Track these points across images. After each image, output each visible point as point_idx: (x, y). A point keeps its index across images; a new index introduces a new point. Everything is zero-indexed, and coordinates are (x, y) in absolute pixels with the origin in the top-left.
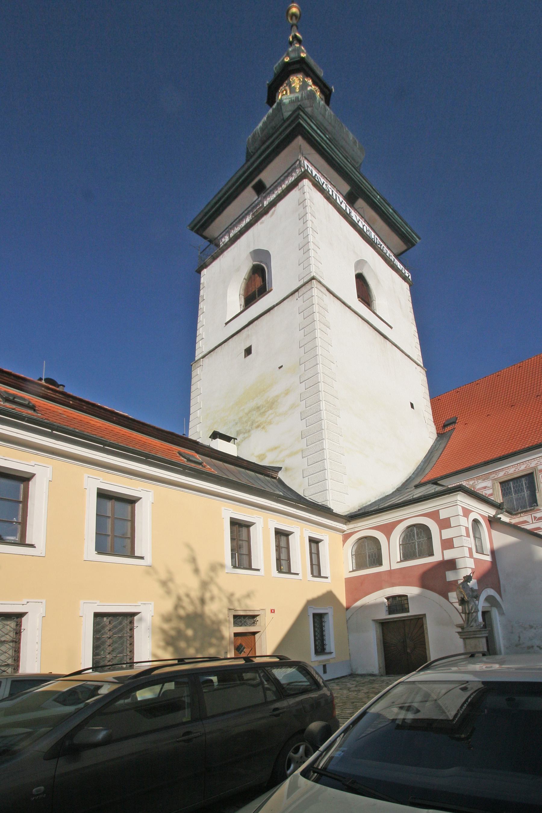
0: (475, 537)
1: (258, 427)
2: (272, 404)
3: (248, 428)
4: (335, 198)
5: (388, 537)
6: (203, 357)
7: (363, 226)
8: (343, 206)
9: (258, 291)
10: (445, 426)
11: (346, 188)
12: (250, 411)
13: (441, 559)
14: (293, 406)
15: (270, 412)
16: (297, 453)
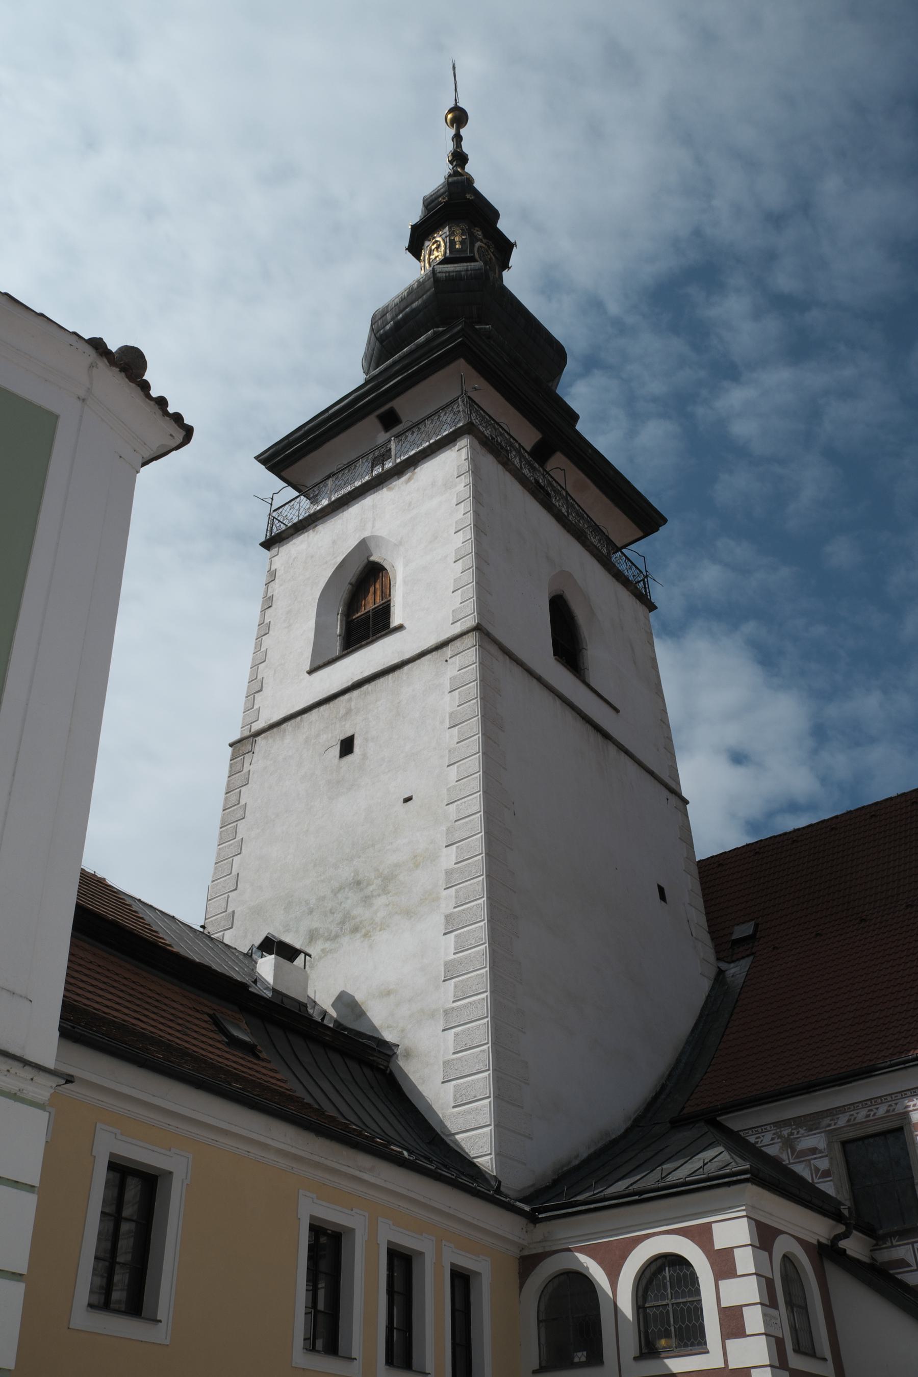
0: (790, 1304)
1: (355, 930)
12: (341, 888)
16: (432, 1015)
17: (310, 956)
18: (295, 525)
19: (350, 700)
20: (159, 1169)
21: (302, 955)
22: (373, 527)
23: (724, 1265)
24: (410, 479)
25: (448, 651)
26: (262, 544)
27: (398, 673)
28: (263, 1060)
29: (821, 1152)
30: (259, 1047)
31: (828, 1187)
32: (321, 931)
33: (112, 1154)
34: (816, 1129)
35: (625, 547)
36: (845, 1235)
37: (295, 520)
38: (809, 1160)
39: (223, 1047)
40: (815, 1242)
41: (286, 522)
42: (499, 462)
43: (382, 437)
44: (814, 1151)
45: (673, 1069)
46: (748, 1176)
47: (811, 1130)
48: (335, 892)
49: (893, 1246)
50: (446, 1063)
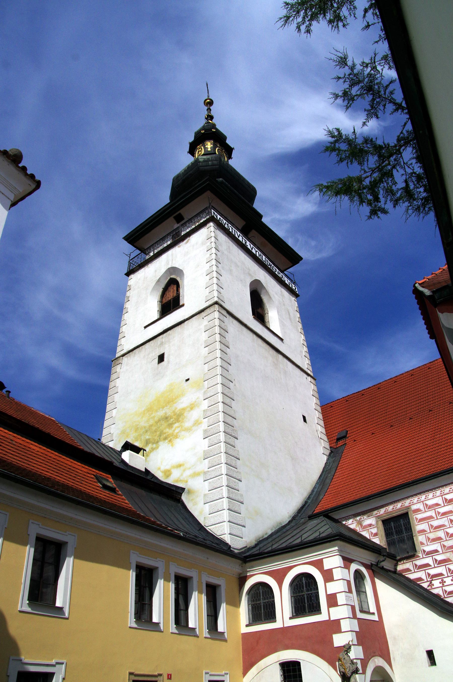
1: (165, 439)
2: (179, 417)
3: (156, 438)
4: (234, 233)
5: (280, 584)
6: (123, 355)
7: (256, 252)
8: (240, 239)
9: (173, 301)
10: (338, 439)
11: (242, 223)
12: (159, 420)
13: (327, 618)
14: (197, 423)
15: (177, 425)
17: (146, 451)
18: (139, 265)
19: (162, 338)
20: (63, 541)
21: (142, 451)
22: (172, 263)
23: (328, 576)
24: (187, 242)
25: (203, 314)
26: (125, 274)
27: (183, 325)
28: (119, 495)
29: (373, 525)
30: (117, 489)
31: (376, 540)
32: (151, 440)
33: (37, 534)
34: (371, 516)
35: (285, 270)
37: (140, 263)
38: (368, 530)
39: (100, 489)
40: (370, 564)
41: (136, 264)
43: (176, 226)
44: (370, 525)
45: (311, 494)
47: (369, 516)
48: (157, 423)
49: (404, 563)
50: (205, 495)
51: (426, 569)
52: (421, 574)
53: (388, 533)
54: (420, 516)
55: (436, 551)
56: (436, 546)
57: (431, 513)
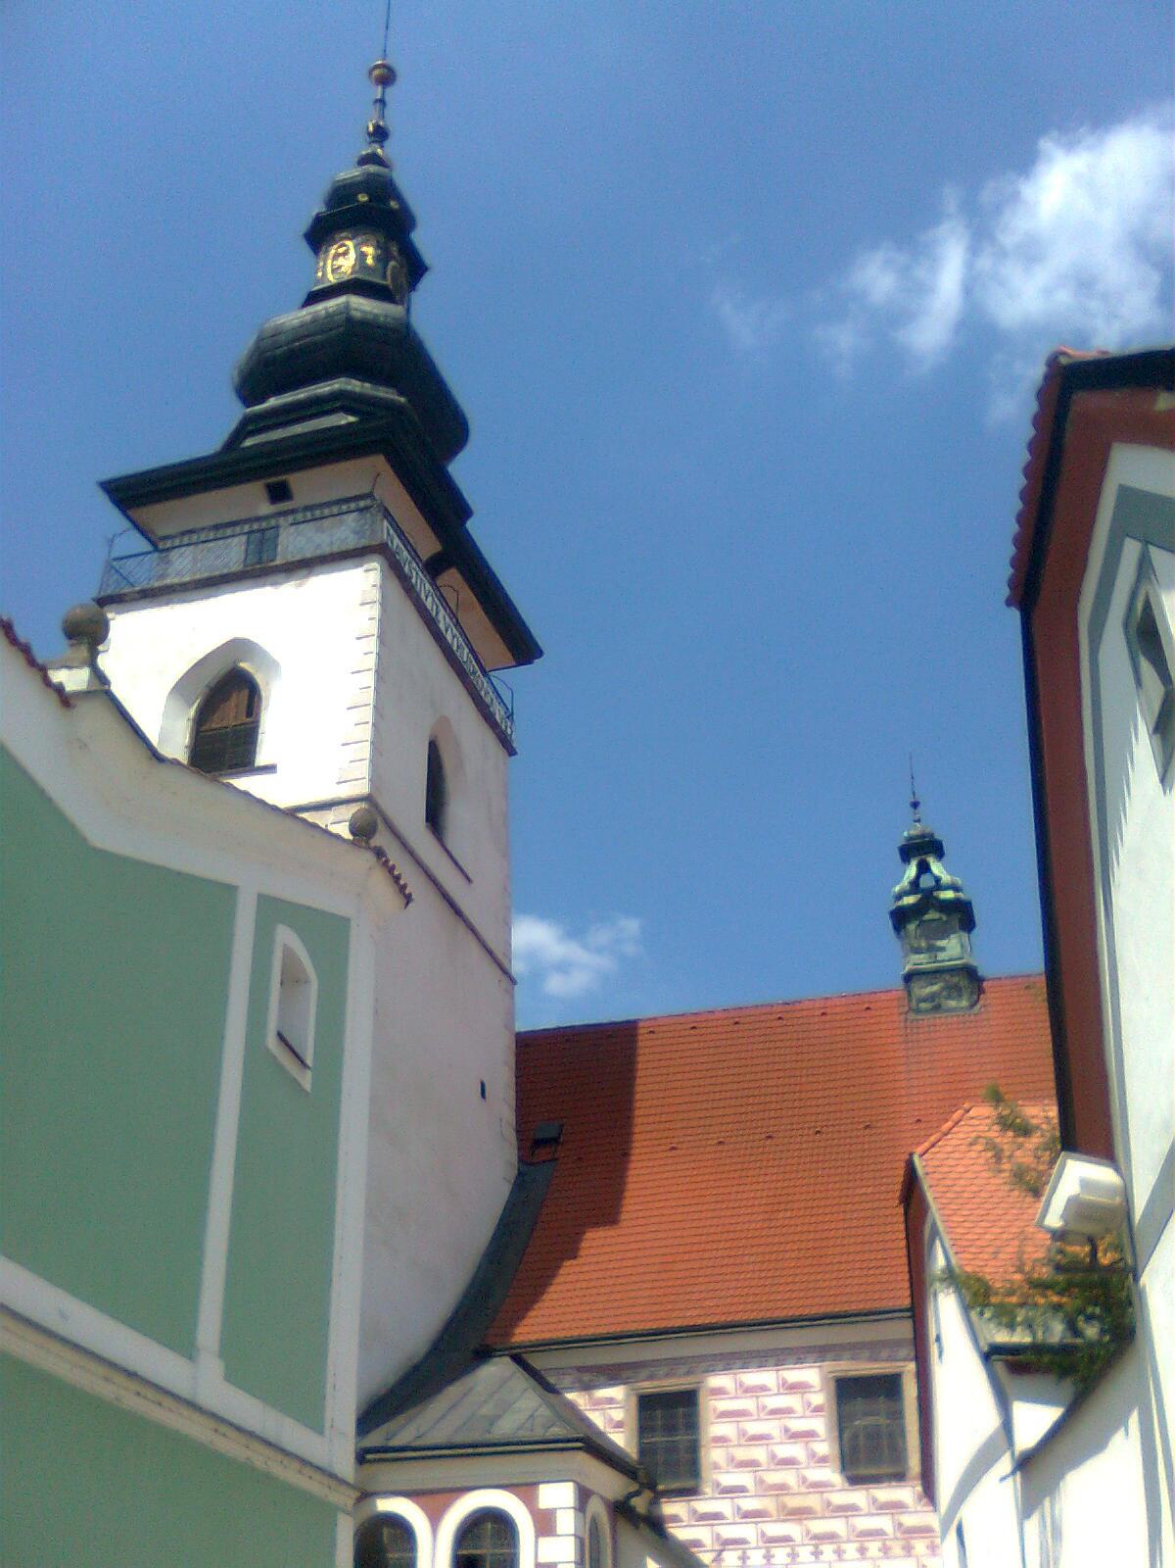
4: (418, 589)
5: (435, 1519)
8: (429, 603)
23: (545, 1524)
36: (637, 1494)
42: (404, 588)
46: (579, 1444)
51: (717, 1525)
52: (701, 1533)
53: (644, 1428)
54: (723, 1405)
55: (742, 1489)
56: (744, 1478)
57: (747, 1404)
